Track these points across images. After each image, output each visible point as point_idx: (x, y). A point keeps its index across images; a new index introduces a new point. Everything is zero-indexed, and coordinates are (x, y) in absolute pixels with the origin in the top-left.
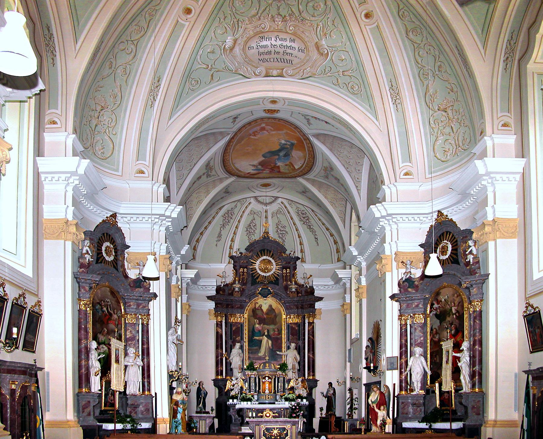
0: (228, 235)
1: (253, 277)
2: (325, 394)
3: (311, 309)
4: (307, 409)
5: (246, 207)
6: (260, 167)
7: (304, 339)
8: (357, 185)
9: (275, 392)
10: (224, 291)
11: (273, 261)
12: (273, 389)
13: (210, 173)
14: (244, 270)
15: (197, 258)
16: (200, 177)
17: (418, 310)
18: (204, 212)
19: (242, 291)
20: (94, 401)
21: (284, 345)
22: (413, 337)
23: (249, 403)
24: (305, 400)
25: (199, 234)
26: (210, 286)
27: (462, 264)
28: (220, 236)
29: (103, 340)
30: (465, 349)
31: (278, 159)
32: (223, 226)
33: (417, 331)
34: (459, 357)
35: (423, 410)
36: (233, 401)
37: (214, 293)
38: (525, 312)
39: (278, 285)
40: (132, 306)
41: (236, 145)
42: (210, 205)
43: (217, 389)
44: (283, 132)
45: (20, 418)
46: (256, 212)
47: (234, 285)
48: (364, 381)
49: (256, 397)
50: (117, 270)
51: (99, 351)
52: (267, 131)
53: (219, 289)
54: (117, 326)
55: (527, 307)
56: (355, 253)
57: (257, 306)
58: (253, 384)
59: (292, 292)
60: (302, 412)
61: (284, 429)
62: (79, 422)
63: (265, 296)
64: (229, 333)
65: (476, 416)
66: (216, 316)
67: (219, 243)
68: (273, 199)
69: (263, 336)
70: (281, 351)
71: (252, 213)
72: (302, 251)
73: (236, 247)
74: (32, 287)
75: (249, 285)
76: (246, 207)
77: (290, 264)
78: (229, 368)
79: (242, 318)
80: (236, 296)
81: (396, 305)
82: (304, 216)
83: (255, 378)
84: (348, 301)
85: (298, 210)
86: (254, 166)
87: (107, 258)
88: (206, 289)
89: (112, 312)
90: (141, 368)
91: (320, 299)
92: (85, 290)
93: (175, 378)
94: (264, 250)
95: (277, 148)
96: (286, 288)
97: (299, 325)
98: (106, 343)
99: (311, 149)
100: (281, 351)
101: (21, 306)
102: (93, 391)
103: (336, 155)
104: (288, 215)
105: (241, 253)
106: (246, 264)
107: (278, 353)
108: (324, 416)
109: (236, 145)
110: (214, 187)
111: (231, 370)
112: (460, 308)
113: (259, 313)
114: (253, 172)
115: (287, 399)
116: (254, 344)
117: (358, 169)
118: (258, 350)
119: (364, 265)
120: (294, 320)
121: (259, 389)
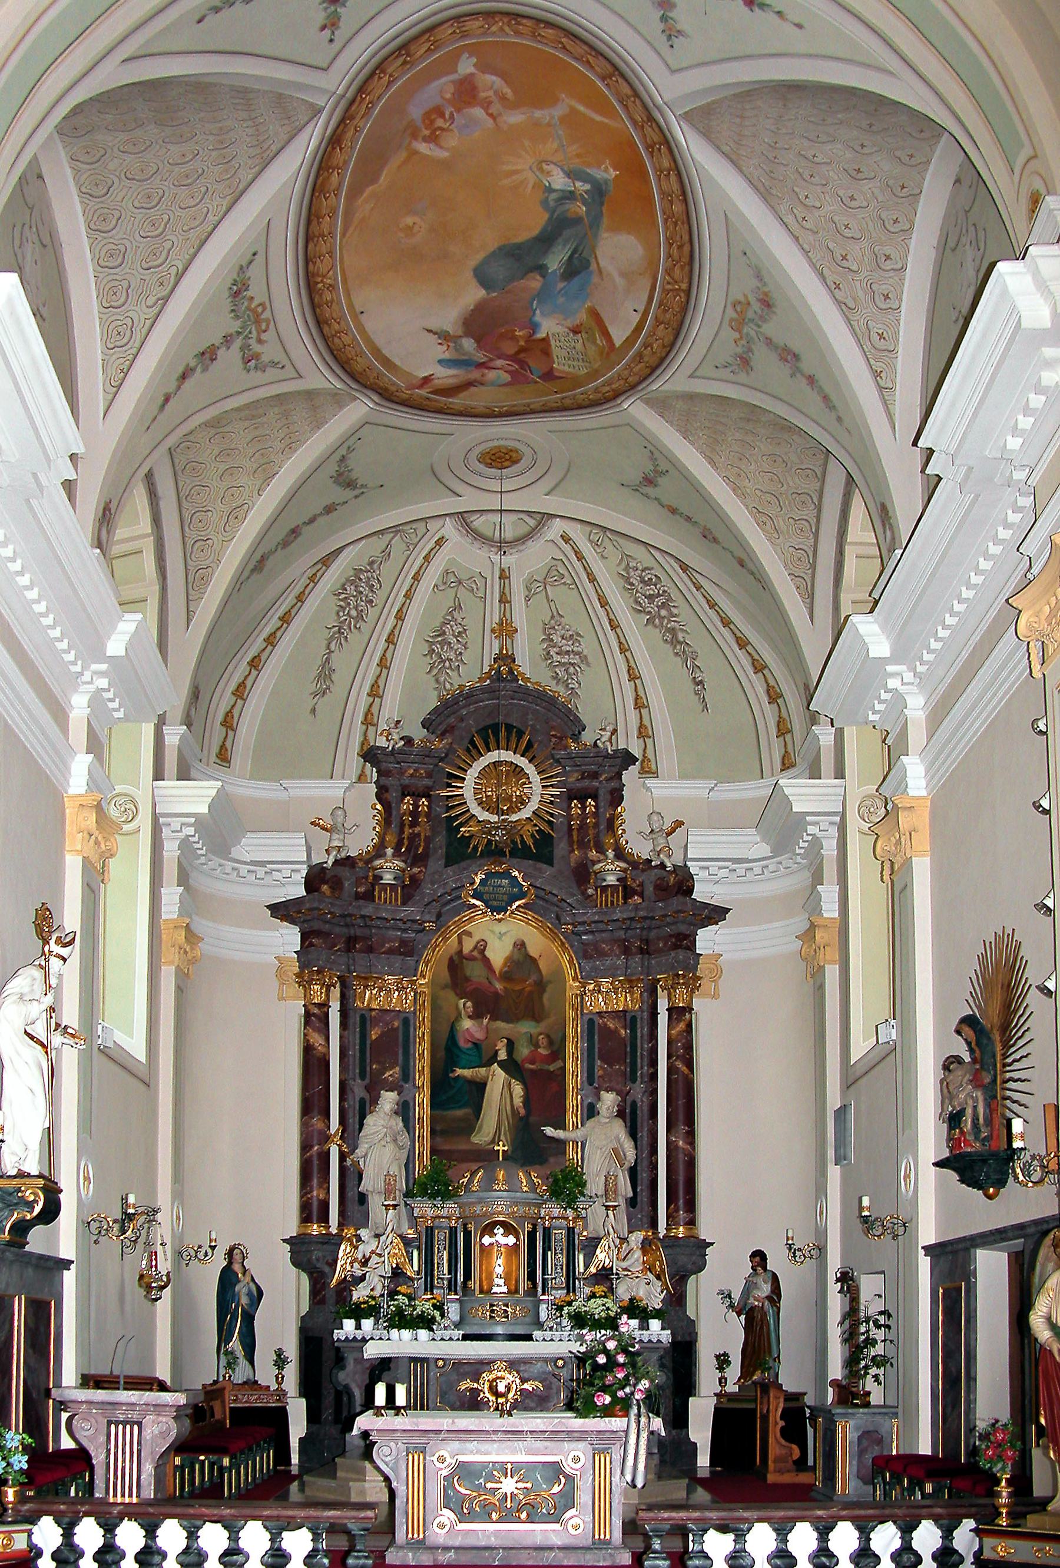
0: (356, 668)
2: (736, 1296)
3: (681, 955)
4: (667, 1361)
5: (427, 559)
6: (468, 344)
7: (654, 1077)
8: (878, 366)
9: (532, 1291)
10: (336, 884)
11: (530, 769)
12: (523, 1273)
13: (256, 348)
14: (416, 806)
15: (237, 760)
16: (208, 355)
18: (258, 564)
19: (409, 889)
21: (573, 1101)
23: (423, 1334)
24: (655, 1324)
25: (243, 667)
26: (281, 860)
28: (326, 673)
32: (340, 633)
36: (358, 1327)
39: (550, 862)
41: (355, 193)
42: (280, 533)
43: (304, 1277)
44: (558, 111)
46: (463, 576)
47: (377, 863)
48: (928, 1234)
49: (453, 1311)
52: (486, 105)
53: (315, 878)
56: (880, 647)
57: (468, 946)
58: (443, 1258)
60: (644, 1384)
61: (555, 1470)
63: (497, 906)
64: (354, 1052)
66: (304, 980)
67: (323, 703)
68: (532, 523)
69: (488, 1064)
70: (561, 1125)
71: (451, 580)
72: (643, 732)
73: (390, 709)
75: (436, 863)
76: (427, 559)
77: (598, 779)
78: (350, 1194)
82: (651, 590)
83: (453, 1231)
84: (830, 910)
85: (627, 568)
86: (444, 337)
88: (268, 880)
91: (716, 914)
93: (31, 1205)
94: (495, 728)
95: (533, 223)
96: (583, 874)
97: (634, 1019)
99: (677, 208)
100: (561, 1125)
103: (789, 219)
105: (409, 741)
106: (427, 782)
107: (549, 1131)
108: (732, 1388)
109: (355, 193)
110: (290, 448)
111: (363, 1199)
113: (475, 972)
114: (445, 375)
115: (580, 1320)
116: (455, 1098)
117: (884, 289)
118: (469, 1126)
119: (916, 707)
120: (608, 997)
121: (467, 1276)
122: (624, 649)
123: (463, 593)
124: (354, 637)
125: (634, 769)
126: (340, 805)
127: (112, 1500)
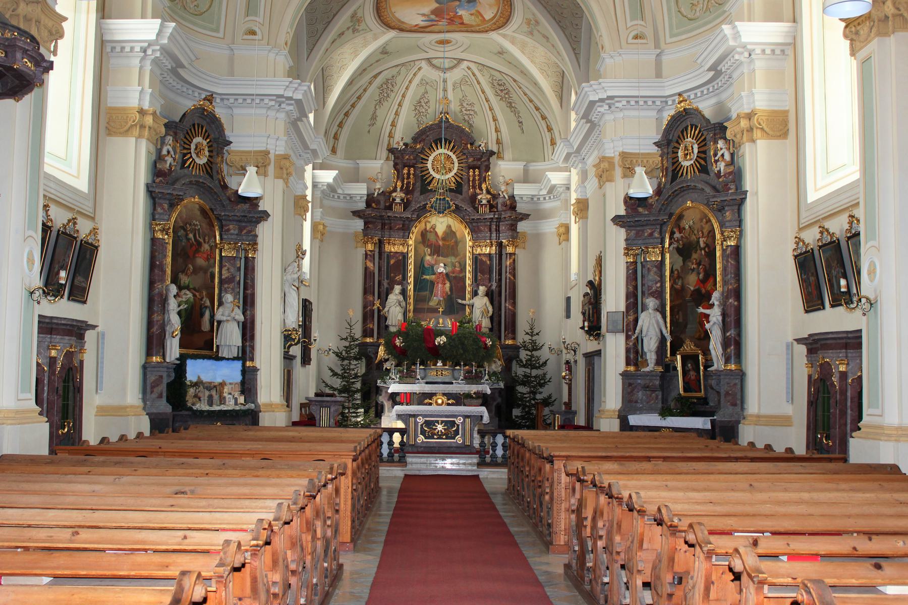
1: (423, 181)
5: (415, 75)
6: (433, 17)
13: (357, 27)
14: (409, 171)
15: (339, 152)
17: (651, 241)
19: (406, 204)
20: (169, 376)
22: (645, 281)
27: (712, 175)
29: (187, 282)
30: (716, 303)
31: (459, 6)
33: (652, 273)
34: (708, 315)
35: (660, 397)
37: (362, 206)
38: (794, 250)
40: (232, 231)
45: (61, 399)
47: (394, 194)
50: (211, 177)
51: (180, 299)
53: (370, 200)
54: (207, 259)
55: (797, 243)
59: (482, 205)
62: (144, 409)
65: (731, 408)
71: (424, 82)
72: (499, 142)
73: (398, 136)
74: (87, 207)
75: (417, 193)
76: (415, 75)
77: (479, 161)
78: (382, 325)
79: (408, 246)
80: (398, 209)
81: (622, 233)
82: (502, 88)
86: (424, 15)
87: (198, 161)
89: (201, 240)
90: (241, 324)
92: (163, 209)
93: (294, 340)
96: (473, 199)
98: (191, 286)
101: (70, 235)
102: (168, 360)
104: (478, 86)
106: (414, 161)
107: (460, 301)
110: (365, 46)
112: (710, 239)
113: (431, 237)
114: (423, 24)
122: (491, 109)
123: (428, 87)
124: (385, 104)
125: (495, 157)
126: (378, 169)
127: (468, 420)
